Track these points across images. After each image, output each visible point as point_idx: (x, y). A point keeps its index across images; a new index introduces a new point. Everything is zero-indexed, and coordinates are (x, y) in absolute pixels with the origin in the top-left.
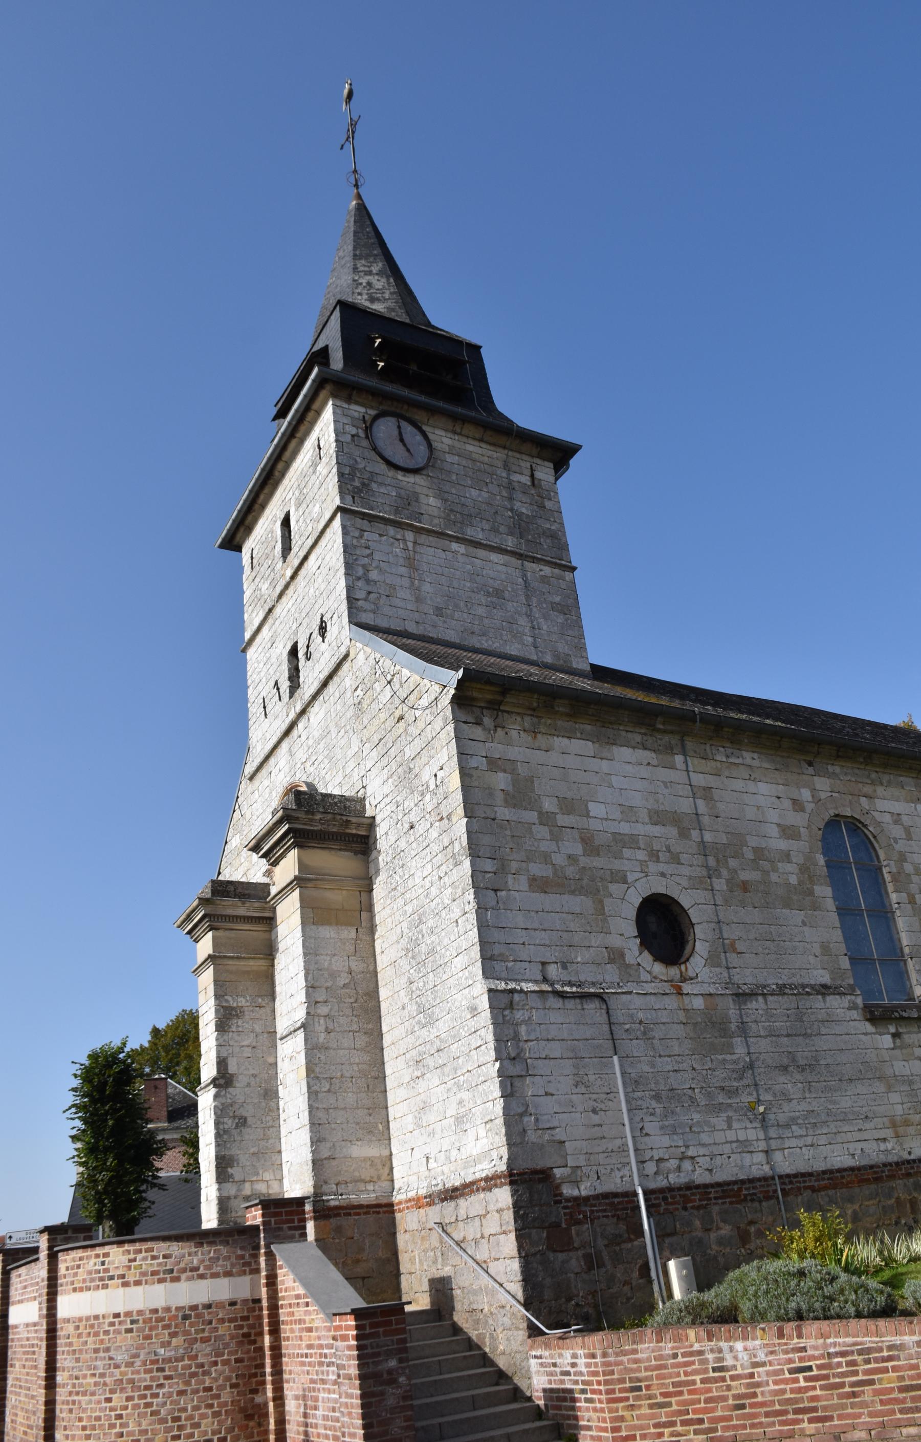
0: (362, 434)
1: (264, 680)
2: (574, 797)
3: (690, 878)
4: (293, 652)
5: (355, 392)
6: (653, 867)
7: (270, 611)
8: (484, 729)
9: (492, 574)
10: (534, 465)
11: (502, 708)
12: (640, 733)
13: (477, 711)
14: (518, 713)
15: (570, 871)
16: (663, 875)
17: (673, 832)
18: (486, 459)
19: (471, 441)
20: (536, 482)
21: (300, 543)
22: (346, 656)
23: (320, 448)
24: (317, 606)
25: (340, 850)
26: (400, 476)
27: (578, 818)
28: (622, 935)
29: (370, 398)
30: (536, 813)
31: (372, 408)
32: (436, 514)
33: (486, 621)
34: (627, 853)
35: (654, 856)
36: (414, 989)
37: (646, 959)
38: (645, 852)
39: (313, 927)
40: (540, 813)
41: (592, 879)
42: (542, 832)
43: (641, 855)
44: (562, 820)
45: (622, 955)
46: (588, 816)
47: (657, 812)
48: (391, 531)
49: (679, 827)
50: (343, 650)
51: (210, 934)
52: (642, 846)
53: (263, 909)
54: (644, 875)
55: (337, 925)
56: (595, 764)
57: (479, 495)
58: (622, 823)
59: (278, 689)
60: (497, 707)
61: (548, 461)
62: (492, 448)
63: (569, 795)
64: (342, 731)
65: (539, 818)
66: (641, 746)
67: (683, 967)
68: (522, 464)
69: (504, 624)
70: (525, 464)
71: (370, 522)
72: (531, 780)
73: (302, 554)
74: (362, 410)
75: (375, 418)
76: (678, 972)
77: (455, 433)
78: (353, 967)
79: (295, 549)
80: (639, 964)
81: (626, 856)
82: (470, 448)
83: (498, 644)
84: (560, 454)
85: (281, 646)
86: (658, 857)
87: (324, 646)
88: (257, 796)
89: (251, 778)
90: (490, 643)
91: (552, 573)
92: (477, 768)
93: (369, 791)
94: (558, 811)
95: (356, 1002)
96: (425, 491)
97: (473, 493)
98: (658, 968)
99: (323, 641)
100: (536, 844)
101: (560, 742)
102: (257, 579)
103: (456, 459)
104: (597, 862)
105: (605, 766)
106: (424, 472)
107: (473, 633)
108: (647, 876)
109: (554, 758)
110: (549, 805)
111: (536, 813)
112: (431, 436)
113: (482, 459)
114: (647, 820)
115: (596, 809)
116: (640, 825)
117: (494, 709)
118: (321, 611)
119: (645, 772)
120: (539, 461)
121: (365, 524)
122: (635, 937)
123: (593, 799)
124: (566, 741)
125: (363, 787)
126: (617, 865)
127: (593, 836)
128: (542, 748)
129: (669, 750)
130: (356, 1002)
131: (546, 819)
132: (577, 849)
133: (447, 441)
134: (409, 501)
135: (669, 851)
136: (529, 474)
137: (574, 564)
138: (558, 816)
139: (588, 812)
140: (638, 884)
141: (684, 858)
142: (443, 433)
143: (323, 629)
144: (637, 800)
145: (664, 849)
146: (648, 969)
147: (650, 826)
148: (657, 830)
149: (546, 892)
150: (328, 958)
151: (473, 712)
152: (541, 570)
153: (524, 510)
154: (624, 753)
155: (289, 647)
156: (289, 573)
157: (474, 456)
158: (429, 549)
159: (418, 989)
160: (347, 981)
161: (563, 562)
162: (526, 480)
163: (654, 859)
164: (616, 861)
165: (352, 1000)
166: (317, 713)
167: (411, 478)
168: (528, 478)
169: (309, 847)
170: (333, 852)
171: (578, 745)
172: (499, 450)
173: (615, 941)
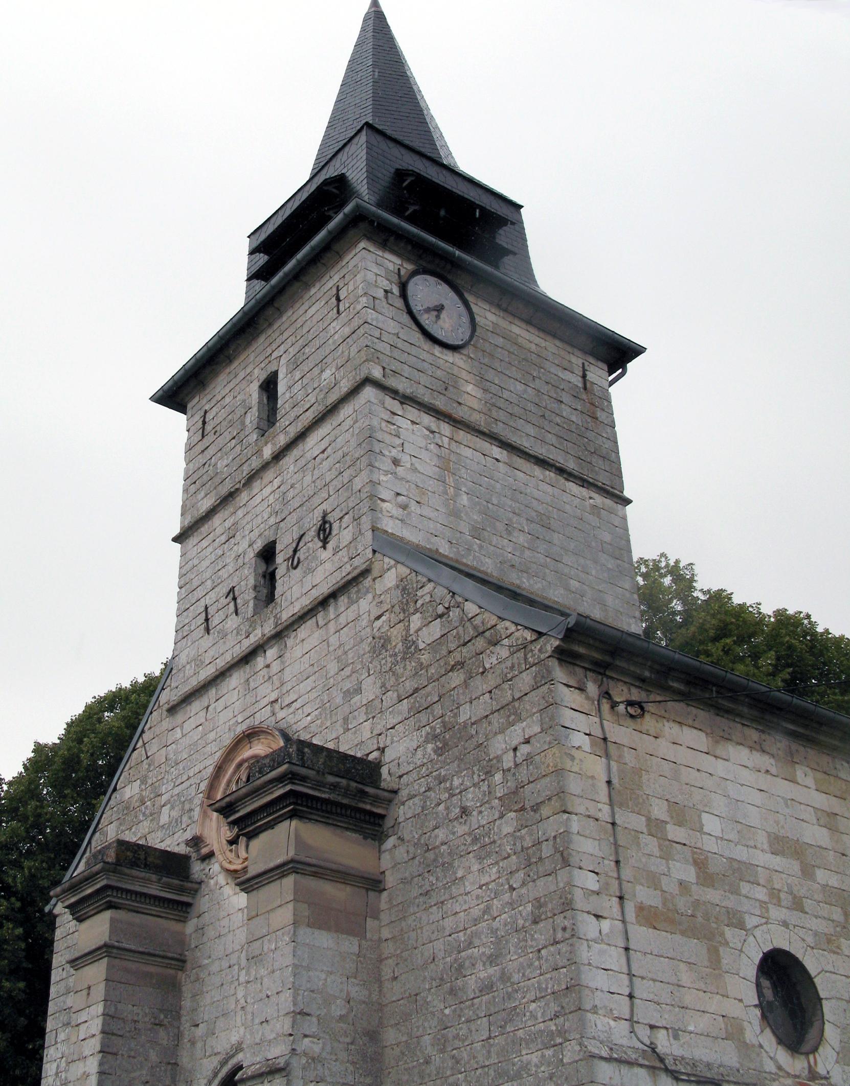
0: (396, 290)
1: (209, 584)
2: (686, 803)
3: (816, 934)
4: (268, 554)
5: (392, 239)
6: (776, 913)
7: (231, 496)
8: (588, 698)
9: (536, 493)
10: (586, 364)
11: (607, 673)
12: (756, 729)
13: (579, 671)
14: (625, 683)
15: (682, 904)
16: (785, 924)
17: (795, 866)
18: (533, 347)
19: (517, 322)
20: (588, 385)
21: (293, 414)
22: (365, 572)
23: (338, 300)
24: (316, 500)
25: (347, 829)
26: (437, 350)
27: (691, 832)
28: (741, 1001)
29: (409, 248)
30: (644, 819)
31: (409, 260)
32: (476, 406)
33: (527, 553)
34: (745, 888)
35: (774, 894)
36: (450, 1036)
37: (768, 1040)
38: (765, 890)
39: (308, 930)
40: (649, 819)
41: (707, 917)
42: (651, 844)
43: (761, 894)
44: (675, 832)
45: (741, 1030)
46: (701, 830)
47: (777, 838)
48: (427, 419)
49: (801, 862)
50: (359, 564)
51: (107, 915)
52: (762, 881)
53: (182, 890)
54: (764, 920)
55: (336, 931)
56: (708, 762)
57: (525, 391)
58: (739, 847)
59: (235, 599)
60: (602, 671)
61: (602, 361)
62: (541, 335)
63: (679, 799)
64: (348, 671)
65: (648, 825)
66: (758, 747)
67: (811, 1057)
68: (574, 359)
69: (548, 560)
70: (577, 360)
71: (402, 403)
72: (638, 772)
73: (293, 431)
74: (398, 261)
75: (414, 274)
76: (806, 1065)
77: (499, 306)
78: (353, 994)
79: (281, 423)
80: (761, 1046)
81: (744, 892)
82: (516, 330)
83: (539, 585)
84: (618, 353)
85: (245, 544)
86: (779, 899)
87: (325, 555)
88: (179, 735)
89: (172, 710)
90: (532, 582)
91: (603, 504)
92: (579, 748)
93: (389, 755)
94: (668, 819)
95: (352, 1043)
96: (464, 375)
97: (518, 387)
98: (783, 1056)
99: (324, 547)
100: (644, 860)
101: (671, 730)
102: (211, 451)
103: (500, 341)
104: (713, 895)
105: (720, 767)
106: (465, 351)
107: (513, 566)
108: (766, 923)
109: (663, 747)
110: (659, 810)
111: (644, 819)
112: (475, 309)
113: (528, 345)
114: (766, 847)
115: (711, 824)
116: (758, 852)
117: (600, 673)
118: (324, 506)
119: (764, 781)
120: (592, 360)
121: (395, 405)
122: (755, 1006)
123: (707, 809)
124: (676, 727)
125: (378, 749)
126: (731, 902)
127: (706, 858)
128: (651, 732)
129: (791, 760)
130: (352, 1043)
131: (656, 827)
132: (689, 874)
133: (491, 317)
134: (448, 385)
135: (791, 893)
136: (581, 374)
137: (627, 493)
138: (668, 826)
139: (702, 826)
140: (758, 933)
141: (808, 904)
142: (487, 307)
143: (324, 532)
144: (753, 817)
145: (786, 889)
146: (772, 1055)
147: (770, 855)
148: (777, 862)
149: (655, 928)
150: (323, 976)
151: (575, 674)
152: (591, 498)
153: (574, 418)
154: (740, 754)
155: (259, 545)
156: (268, 452)
157: (520, 340)
158: (467, 449)
159: (456, 1037)
160: (344, 1012)
161: (616, 492)
162: (577, 381)
163: (775, 901)
164: (732, 897)
165: (348, 1040)
166: (307, 638)
167: (449, 356)
168: (580, 379)
169: (310, 819)
170: (338, 831)
171: (692, 737)
172: (548, 338)
173: (734, 1010)
